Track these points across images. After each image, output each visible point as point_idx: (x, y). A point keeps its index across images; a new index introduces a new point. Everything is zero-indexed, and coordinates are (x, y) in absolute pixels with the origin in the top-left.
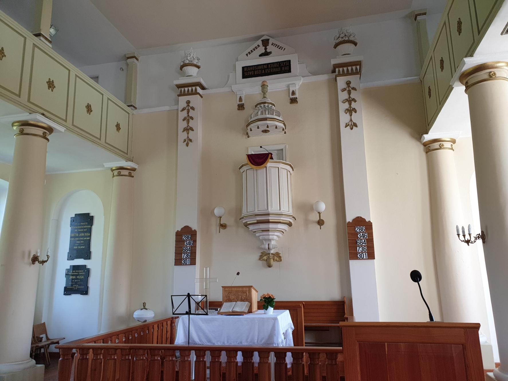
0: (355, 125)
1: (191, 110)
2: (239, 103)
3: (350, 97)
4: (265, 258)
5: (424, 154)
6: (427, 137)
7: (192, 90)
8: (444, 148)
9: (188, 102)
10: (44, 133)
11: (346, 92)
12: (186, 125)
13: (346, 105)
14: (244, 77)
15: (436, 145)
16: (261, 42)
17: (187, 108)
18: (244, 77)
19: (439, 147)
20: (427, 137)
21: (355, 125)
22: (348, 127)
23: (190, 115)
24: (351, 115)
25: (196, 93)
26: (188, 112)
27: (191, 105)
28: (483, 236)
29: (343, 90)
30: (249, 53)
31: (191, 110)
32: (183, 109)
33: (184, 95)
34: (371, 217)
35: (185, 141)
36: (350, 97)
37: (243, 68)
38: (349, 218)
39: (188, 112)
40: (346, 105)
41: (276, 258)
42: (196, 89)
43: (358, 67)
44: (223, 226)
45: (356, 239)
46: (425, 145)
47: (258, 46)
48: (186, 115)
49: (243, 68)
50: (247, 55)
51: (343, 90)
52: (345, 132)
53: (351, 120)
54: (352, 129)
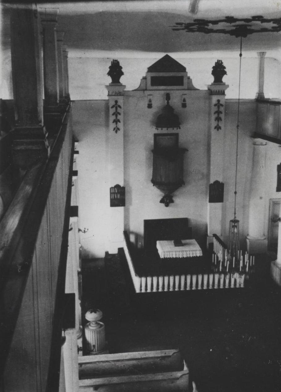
1: (118, 115)
9: (116, 102)
11: (216, 107)
17: (115, 106)
18: (153, 84)
29: (215, 105)
31: (118, 115)
32: (112, 107)
38: (212, 182)
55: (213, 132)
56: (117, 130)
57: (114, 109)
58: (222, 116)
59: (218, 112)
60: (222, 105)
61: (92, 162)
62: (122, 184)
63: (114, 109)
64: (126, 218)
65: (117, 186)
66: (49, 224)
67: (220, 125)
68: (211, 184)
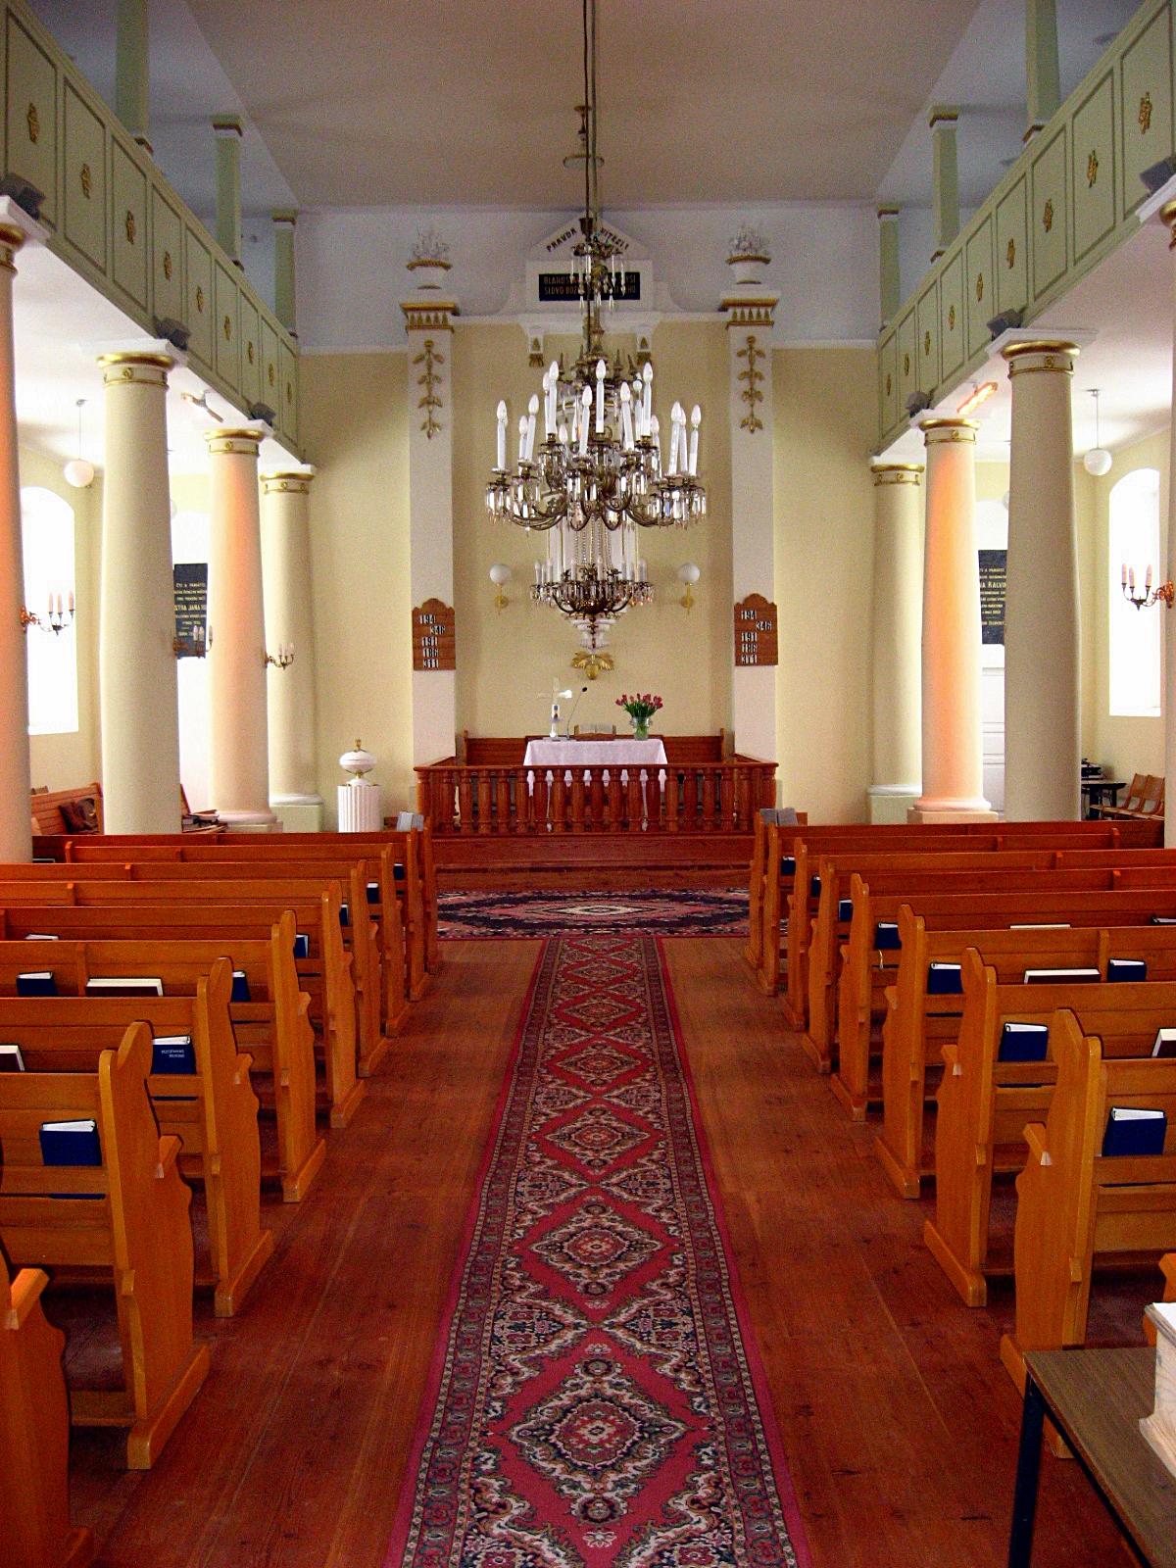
0: (759, 425)
1: (435, 362)
2: (639, 350)
3: (752, 370)
4: (584, 662)
5: (871, 487)
6: (879, 461)
7: (436, 318)
8: (904, 482)
9: (751, 340)
10: (1048, 360)
11: (745, 359)
12: (425, 394)
13: (745, 385)
14: (544, 296)
15: (891, 476)
16: (579, 224)
17: (427, 357)
18: (544, 296)
19: (894, 479)
20: (879, 461)
21: (759, 425)
22: (746, 428)
23: (433, 372)
24: (752, 406)
25: (445, 326)
26: (430, 367)
27: (756, 346)
28: (1166, 595)
29: (741, 354)
30: (554, 244)
31: (435, 362)
33: (742, 323)
34: (775, 598)
35: (424, 428)
36: (752, 370)
37: (542, 277)
38: (739, 595)
39: (430, 367)
40: (745, 385)
41: (603, 663)
42: (445, 318)
43: (769, 310)
44: (504, 602)
45: (754, 632)
46: (874, 470)
47: (573, 231)
48: (425, 372)
49: (542, 277)
50: (549, 248)
51: (741, 354)
52: (739, 436)
53: (752, 415)
54: (752, 431)
55: (739, 436)
56: (430, 427)
57: (423, 366)
58: (763, 386)
59: (751, 375)
60: (760, 353)
61: (390, 1307)
62: (449, 603)
63: (423, 366)
64: (465, 701)
65: (434, 604)
66: (109, 197)
67: (757, 368)
68: (738, 604)
